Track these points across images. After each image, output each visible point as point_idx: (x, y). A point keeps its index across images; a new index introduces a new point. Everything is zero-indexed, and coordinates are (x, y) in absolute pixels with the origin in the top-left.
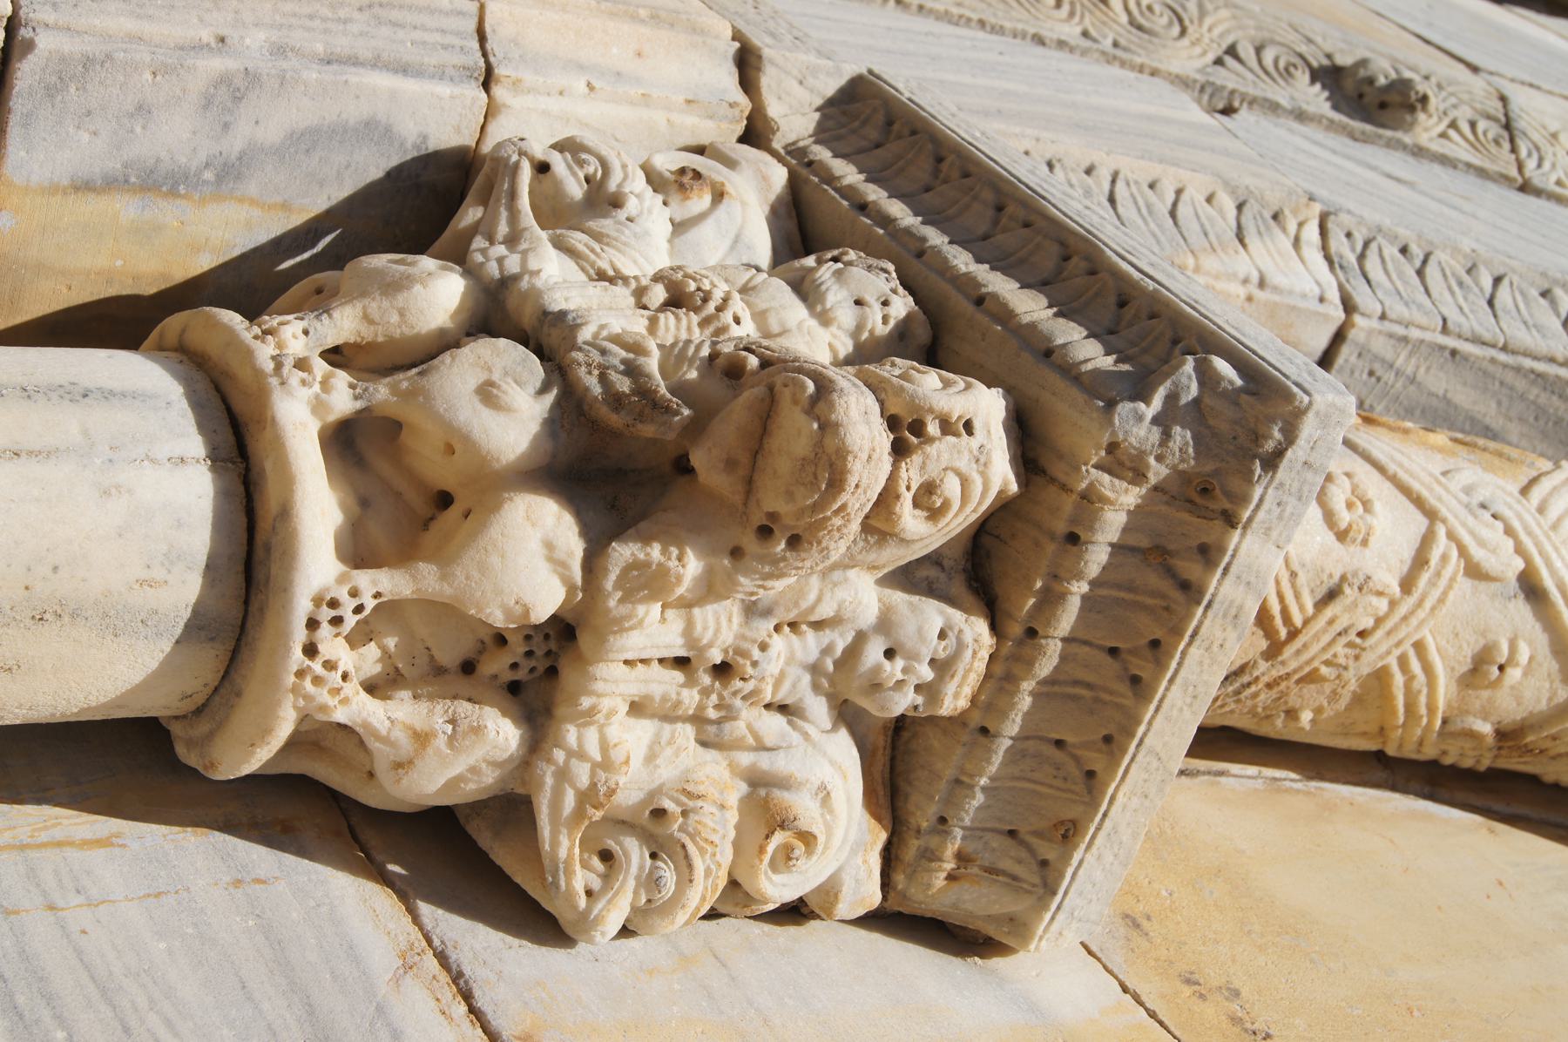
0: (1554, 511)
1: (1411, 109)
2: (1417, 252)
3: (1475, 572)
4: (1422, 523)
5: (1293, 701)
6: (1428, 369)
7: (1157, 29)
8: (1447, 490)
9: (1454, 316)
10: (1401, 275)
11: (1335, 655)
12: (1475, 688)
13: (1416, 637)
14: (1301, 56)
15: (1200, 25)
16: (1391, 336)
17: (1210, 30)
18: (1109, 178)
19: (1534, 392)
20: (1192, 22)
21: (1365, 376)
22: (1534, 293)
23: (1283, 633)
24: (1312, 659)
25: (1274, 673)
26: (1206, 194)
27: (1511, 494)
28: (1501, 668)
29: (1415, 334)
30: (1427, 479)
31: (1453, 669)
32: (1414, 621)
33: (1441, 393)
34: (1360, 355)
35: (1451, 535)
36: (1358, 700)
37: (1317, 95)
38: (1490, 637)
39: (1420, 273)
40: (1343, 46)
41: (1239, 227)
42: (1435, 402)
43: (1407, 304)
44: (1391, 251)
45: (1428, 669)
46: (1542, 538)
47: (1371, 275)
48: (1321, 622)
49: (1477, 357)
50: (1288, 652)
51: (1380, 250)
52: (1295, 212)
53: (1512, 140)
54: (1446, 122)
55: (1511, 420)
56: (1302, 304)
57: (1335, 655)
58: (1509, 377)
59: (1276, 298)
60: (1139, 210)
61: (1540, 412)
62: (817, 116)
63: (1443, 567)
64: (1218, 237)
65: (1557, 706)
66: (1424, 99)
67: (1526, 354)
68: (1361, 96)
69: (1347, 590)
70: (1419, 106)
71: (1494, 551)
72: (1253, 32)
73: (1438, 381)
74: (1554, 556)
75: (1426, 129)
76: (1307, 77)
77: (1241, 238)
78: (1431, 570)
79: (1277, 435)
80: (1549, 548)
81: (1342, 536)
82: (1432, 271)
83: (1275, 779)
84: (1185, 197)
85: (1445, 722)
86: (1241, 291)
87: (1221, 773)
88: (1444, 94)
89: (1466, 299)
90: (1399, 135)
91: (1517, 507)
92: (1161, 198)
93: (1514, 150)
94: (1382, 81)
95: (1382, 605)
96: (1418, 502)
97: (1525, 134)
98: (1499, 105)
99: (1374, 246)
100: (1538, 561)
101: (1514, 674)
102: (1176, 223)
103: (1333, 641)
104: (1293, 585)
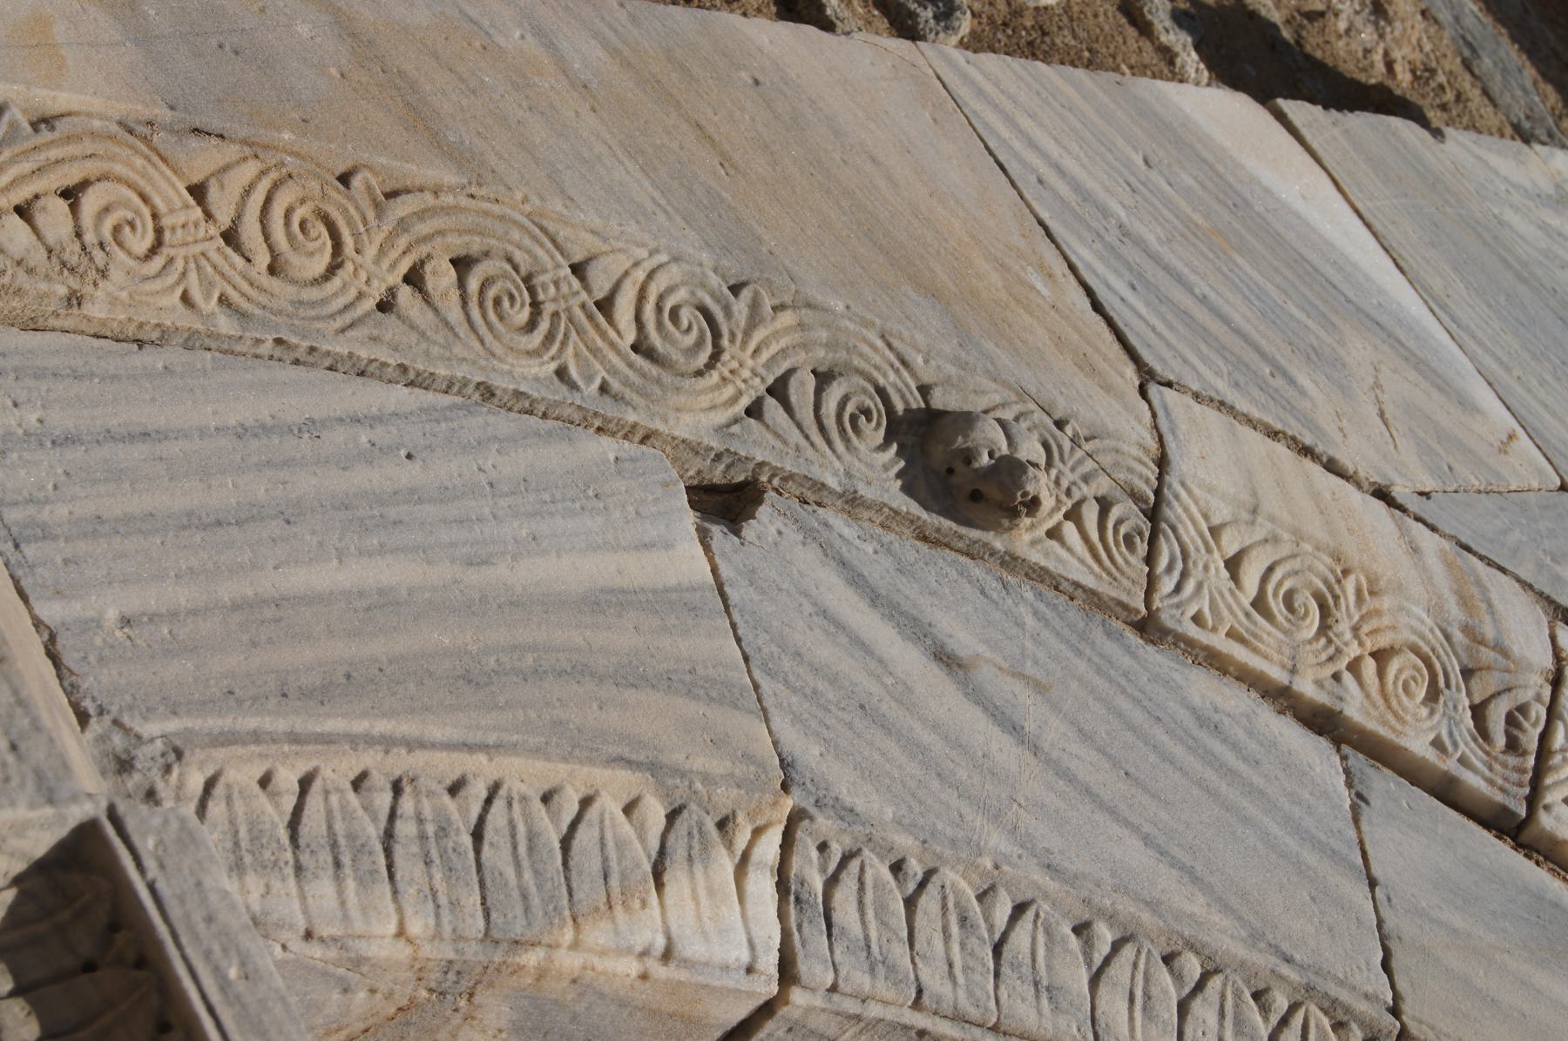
1: (1014, 514)
2: (915, 868)
7: (676, 356)
9: (935, 981)
10: (881, 909)
14: (881, 392)
15: (744, 343)
17: (756, 352)
18: (484, 794)
22: (1067, 930)
26: (626, 799)
29: (874, 1010)
34: (790, 1030)
37: (886, 468)
39: (910, 903)
40: (951, 370)
43: (872, 970)
47: (837, 917)
51: (862, 869)
52: (751, 816)
53: (1152, 542)
59: (682, 975)
60: (515, 847)
62: (10, 895)
64: (624, 877)
72: (821, 353)
77: (658, 874)
82: (929, 903)
84: (592, 813)
88: (1079, 454)
89: (963, 945)
90: (989, 537)
93: (1150, 559)
94: (985, 460)
98: (1151, 472)
99: (854, 865)
102: (565, 863)
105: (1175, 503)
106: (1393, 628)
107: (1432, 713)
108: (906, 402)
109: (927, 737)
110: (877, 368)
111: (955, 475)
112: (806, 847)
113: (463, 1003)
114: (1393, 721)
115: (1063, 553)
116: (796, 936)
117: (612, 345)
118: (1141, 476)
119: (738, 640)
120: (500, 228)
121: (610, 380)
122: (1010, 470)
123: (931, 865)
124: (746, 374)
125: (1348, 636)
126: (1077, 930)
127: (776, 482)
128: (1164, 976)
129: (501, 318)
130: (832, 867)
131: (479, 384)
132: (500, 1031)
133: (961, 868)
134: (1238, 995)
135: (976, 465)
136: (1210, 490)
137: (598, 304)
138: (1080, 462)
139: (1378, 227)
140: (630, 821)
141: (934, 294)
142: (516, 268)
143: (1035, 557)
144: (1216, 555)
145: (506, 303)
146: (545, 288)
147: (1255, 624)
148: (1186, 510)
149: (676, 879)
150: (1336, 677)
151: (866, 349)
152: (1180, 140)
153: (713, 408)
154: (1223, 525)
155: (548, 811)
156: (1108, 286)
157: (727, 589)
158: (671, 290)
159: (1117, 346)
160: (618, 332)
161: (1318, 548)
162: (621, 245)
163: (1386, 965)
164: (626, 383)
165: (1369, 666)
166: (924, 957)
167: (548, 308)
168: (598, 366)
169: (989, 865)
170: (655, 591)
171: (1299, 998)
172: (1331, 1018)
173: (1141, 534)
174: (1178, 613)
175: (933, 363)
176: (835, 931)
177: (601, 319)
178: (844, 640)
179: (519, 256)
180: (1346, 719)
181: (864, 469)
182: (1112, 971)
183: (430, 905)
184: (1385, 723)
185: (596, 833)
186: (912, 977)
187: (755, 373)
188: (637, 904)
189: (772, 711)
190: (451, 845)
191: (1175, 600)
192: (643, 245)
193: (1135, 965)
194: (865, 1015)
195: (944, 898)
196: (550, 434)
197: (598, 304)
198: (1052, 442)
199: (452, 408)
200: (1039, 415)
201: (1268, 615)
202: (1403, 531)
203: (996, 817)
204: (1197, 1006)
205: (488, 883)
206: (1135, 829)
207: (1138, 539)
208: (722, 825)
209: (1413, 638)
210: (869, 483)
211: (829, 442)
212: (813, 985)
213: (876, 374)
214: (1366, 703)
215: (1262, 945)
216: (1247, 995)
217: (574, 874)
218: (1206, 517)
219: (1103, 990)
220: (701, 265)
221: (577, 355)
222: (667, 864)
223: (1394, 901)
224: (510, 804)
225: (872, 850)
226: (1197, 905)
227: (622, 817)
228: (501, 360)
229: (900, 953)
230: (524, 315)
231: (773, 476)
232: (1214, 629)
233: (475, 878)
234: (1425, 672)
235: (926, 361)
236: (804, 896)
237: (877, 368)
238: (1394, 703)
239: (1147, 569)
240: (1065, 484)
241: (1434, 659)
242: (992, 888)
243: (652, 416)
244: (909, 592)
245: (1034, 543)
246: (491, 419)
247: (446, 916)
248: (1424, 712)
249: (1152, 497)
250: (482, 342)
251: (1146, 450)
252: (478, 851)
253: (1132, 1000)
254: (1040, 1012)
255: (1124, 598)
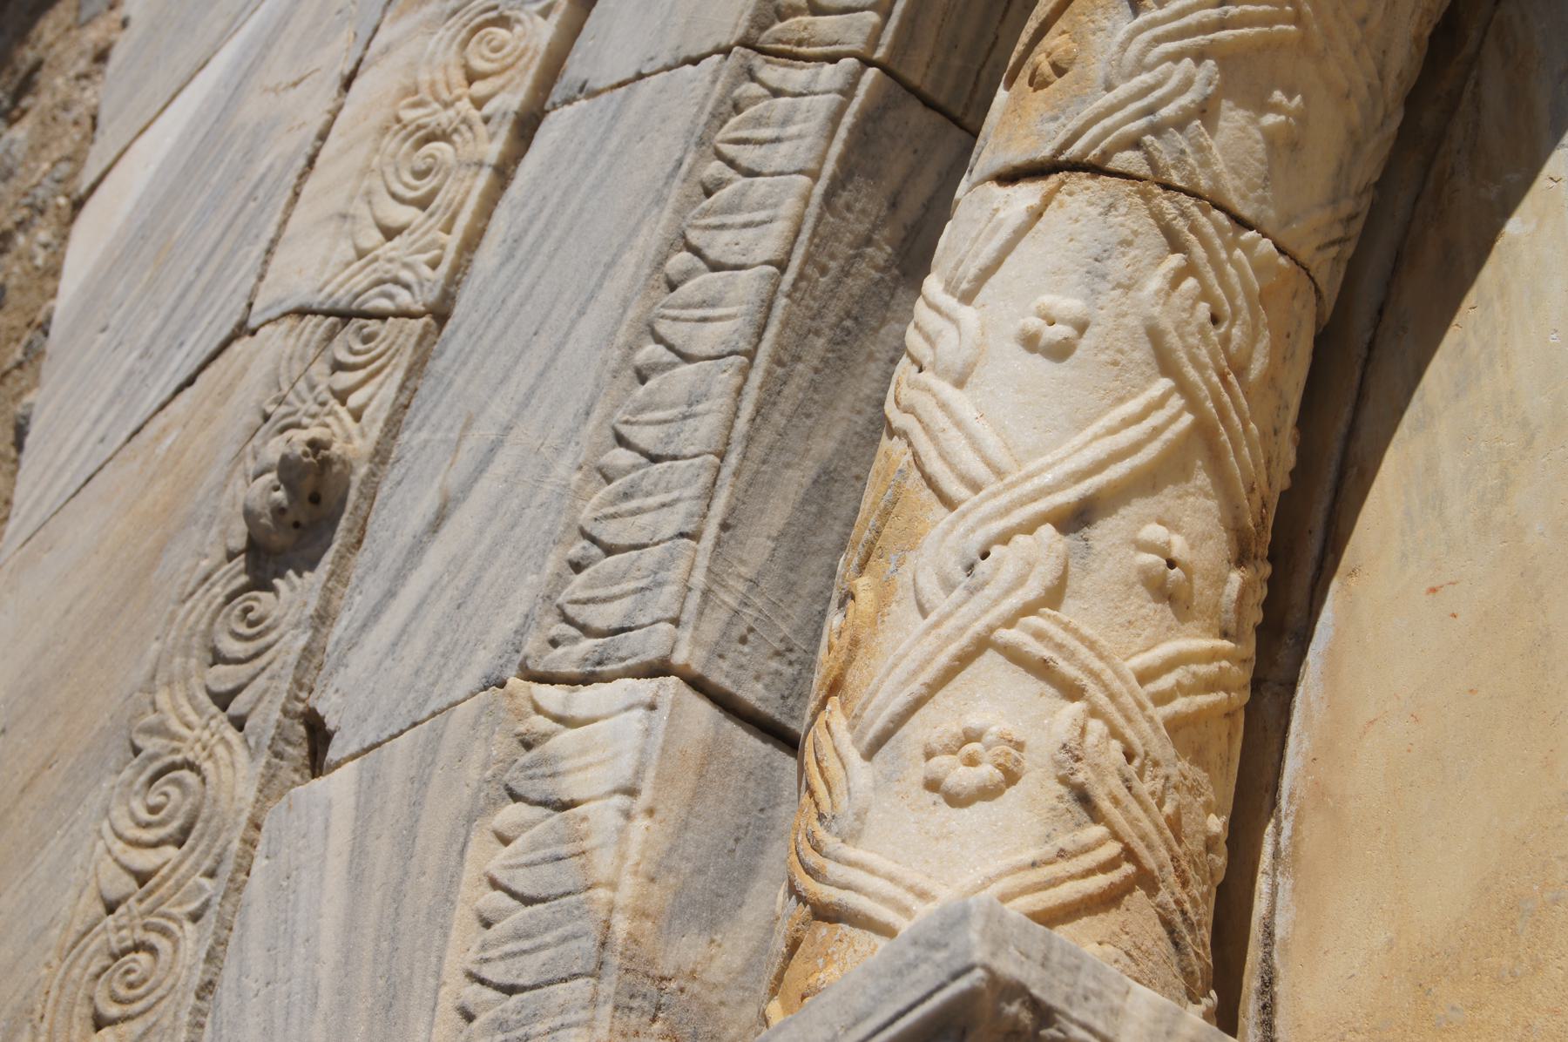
0: (979, 470)
1: (326, 463)
2: (578, 548)
3: (1054, 596)
4: (990, 657)
5: (1196, 845)
6: (742, 562)
7: (186, 807)
8: (949, 615)
9: (674, 520)
10: (612, 579)
11: (1153, 794)
12: (1191, 595)
13: (1134, 682)
14: (230, 598)
15: (182, 739)
16: (701, 613)
17: (189, 726)
18: (477, 986)
19: (777, 418)
20: (176, 751)
21: (746, 649)
22: (640, 391)
23: (1128, 868)
24: (1157, 826)
25: (1172, 879)
26: (496, 844)
27: (953, 525)
28: (1171, 564)
29: (699, 579)
30: (930, 643)
31: (1169, 629)
32: (1117, 685)
33: (771, 544)
34: (721, 656)
35: (1010, 622)
36: (1198, 756)
37: (293, 588)
38: (1133, 577)
39: (609, 550)
40: (214, 531)
41: (544, 804)
42: (781, 553)
43: (660, 584)
44: (578, 585)
45: (1169, 665)
46: (1016, 493)
48: (1115, 814)
49: (732, 494)
50: (1150, 863)
51: (576, 602)
52: (521, 717)
53: (368, 315)
54: (334, 404)
55: (808, 450)
56: (658, 739)
57: (1153, 794)
58: (757, 451)
59: (650, 774)
60: (524, 952)
61: (801, 411)
63: (1051, 639)
64: (561, 841)
65: (1213, 484)
66: (315, 445)
67: (730, 427)
68: (296, 525)
69: (1080, 778)
70: (323, 452)
71: (1030, 565)
72: (193, 662)
73: (756, 547)
74: (1037, 482)
75: (353, 442)
76: (265, 596)
78: (1054, 656)
79: (1013, 1009)
80: (1028, 487)
81: (1011, 777)
83: (1276, 855)
84: (502, 877)
85: (1225, 635)
86: (641, 823)
87: (1269, 933)
88: (291, 397)
89: (648, 494)
90: (356, 480)
91: (971, 519)
92: (504, 913)
93: (382, 316)
94: (280, 495)
95: (1096, 727)
96: (964, 659)
97: (357, 296)
98: (311, 321)
99: (571, 610)
100: (1042, 505)
101: (1179, 546)
102: (543, 900)
103: (1137, 797)
104: (1075, 855)
105: (336, 296)
106: (446, 67)
107: (519, 21)
108: (239, 573)
109: (487, 540)
110: (209, 605)
111: (303, 518)
112: (552, 660)
113: (673, 985)
114: (525, 59)
115: (374, 404)
116: (629, 662)
117: (174, 869)
118: (313, 333)
119: (402, 732)
120: (70, 988)
121: (203, 868)
122: (288, 470)
123: (576, 532)
124: (206, 735)
125: (451, 112)
126: (643, 380)
127: (303, 695)
128: (685, 290)
129: (144, 980)
130: (573, 632)
131: (199, 997)
132: (712, 941)
133: (580, 503)
134: (706, 213)
135: (285, 503)
136: (325, 262)
137: (141, 885)
138: (298, 395)
139: (174, 88)
140: (515, 838)
141: (161, 548)
142: (105, 969)
143: (375, 432)
144: (379, 252)
145: (132, 977)
146: (122, 940)
147: (438, 207)
148: (341, 285)
149: (568, 788)
150: (486, 120)
151: (192, 618)
152: (95, 292)
153: (233, 765)
154: (356, 247)
155: (497, 921)
156: (177, 370)
157: (366, 745)
158: (132, 815)
159: (220, 361)
160: (165, 864)
161: (377, 150)
162: (91, 868)
163: (695, 61)
164: (207, 852)
165: (480, 88)
166: (654, 533)
167: (140, 935)
168: (190, 882)
169: (579, 475)
170: (357, 819)
171: (710, 151)
172: (730, 116)
173: (361, 328)
174: (428, 285)
175: (207, 550)
176: (627, 624)
177: (151, 883)
178: (414, 624)
179: (94, 968)
180: (524, 106)
181: (293, 610)
182: (678, 342)
183: (561, 1033)
184: (527, 68)
185: (521, 871)
186: (669, 543)
187: (207, 726)
188: (584, 826)
189: (451, 699)
190: (514, 1017)
191: (416, 288)
192: (94, 845)
193: (675, 319)
194: (702, 586)
195: (606, 517)
196: (242, 925)
197: (141, 885)
198: (279, 425)
199: (214, 1023)
200: (256, 441)
201: (433, 194)
202: (375, 63)
203: (547, 468)
204: (713, 254)
205: (550, 976)
206: (573, 323)
207: (366, 331)
208: (528, 746)
209: (455, 47)
210: (305, 604)
211: (268, 647)
212: (670, 643)
213: (214, 606)
214: (509, 89)
215: (666, 191)
216: (707, 203)
217: (552, 891)
218: (348, 264)
219: (694, 349)
220: (113, 788)
221: (180, 904)
222: (554, 798)
223: (652, 54)
224: (487, 960)
225: (559, 593)
226: (630, 259)
227: (512, 846)
228: (178, 978)
229: (650, 557)
230: (143, 957)
231: (297, 698)
232: (443, 247)
233: (546, 989)
234: (483, 32)
235: (206, 556)
236: (596, 657)
237: (209, 605)
238: (510, 60)
239: (391, 319)
240: (315, 408)
241: (473, 24)
242: (599, 470)
243: (236, 824)
244: (391, 559)
245: (363, 435)
246: (225, 984)
247: (571, 1017)
248: (518, 29)
249: (332, 319)
250: (162, 998)
251: (292, 329)
252: (523, 989)
253: (704, 320)
254: (707, 413)
255: (414, 340)
